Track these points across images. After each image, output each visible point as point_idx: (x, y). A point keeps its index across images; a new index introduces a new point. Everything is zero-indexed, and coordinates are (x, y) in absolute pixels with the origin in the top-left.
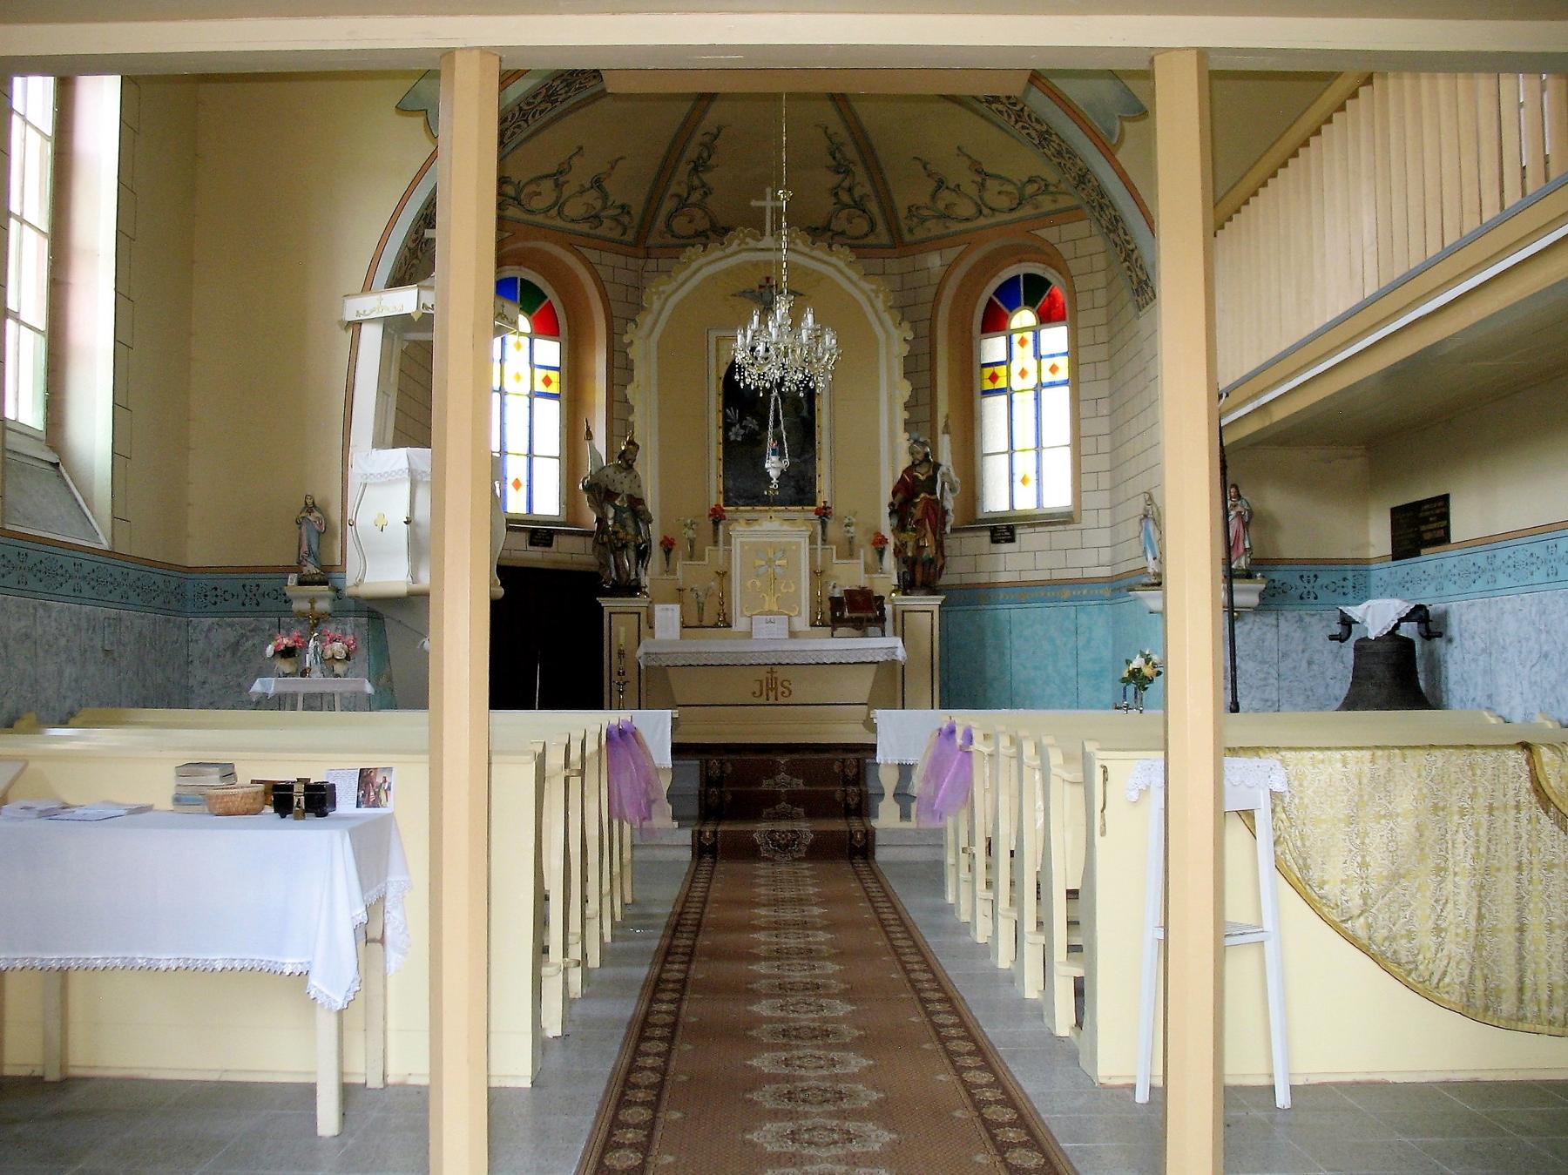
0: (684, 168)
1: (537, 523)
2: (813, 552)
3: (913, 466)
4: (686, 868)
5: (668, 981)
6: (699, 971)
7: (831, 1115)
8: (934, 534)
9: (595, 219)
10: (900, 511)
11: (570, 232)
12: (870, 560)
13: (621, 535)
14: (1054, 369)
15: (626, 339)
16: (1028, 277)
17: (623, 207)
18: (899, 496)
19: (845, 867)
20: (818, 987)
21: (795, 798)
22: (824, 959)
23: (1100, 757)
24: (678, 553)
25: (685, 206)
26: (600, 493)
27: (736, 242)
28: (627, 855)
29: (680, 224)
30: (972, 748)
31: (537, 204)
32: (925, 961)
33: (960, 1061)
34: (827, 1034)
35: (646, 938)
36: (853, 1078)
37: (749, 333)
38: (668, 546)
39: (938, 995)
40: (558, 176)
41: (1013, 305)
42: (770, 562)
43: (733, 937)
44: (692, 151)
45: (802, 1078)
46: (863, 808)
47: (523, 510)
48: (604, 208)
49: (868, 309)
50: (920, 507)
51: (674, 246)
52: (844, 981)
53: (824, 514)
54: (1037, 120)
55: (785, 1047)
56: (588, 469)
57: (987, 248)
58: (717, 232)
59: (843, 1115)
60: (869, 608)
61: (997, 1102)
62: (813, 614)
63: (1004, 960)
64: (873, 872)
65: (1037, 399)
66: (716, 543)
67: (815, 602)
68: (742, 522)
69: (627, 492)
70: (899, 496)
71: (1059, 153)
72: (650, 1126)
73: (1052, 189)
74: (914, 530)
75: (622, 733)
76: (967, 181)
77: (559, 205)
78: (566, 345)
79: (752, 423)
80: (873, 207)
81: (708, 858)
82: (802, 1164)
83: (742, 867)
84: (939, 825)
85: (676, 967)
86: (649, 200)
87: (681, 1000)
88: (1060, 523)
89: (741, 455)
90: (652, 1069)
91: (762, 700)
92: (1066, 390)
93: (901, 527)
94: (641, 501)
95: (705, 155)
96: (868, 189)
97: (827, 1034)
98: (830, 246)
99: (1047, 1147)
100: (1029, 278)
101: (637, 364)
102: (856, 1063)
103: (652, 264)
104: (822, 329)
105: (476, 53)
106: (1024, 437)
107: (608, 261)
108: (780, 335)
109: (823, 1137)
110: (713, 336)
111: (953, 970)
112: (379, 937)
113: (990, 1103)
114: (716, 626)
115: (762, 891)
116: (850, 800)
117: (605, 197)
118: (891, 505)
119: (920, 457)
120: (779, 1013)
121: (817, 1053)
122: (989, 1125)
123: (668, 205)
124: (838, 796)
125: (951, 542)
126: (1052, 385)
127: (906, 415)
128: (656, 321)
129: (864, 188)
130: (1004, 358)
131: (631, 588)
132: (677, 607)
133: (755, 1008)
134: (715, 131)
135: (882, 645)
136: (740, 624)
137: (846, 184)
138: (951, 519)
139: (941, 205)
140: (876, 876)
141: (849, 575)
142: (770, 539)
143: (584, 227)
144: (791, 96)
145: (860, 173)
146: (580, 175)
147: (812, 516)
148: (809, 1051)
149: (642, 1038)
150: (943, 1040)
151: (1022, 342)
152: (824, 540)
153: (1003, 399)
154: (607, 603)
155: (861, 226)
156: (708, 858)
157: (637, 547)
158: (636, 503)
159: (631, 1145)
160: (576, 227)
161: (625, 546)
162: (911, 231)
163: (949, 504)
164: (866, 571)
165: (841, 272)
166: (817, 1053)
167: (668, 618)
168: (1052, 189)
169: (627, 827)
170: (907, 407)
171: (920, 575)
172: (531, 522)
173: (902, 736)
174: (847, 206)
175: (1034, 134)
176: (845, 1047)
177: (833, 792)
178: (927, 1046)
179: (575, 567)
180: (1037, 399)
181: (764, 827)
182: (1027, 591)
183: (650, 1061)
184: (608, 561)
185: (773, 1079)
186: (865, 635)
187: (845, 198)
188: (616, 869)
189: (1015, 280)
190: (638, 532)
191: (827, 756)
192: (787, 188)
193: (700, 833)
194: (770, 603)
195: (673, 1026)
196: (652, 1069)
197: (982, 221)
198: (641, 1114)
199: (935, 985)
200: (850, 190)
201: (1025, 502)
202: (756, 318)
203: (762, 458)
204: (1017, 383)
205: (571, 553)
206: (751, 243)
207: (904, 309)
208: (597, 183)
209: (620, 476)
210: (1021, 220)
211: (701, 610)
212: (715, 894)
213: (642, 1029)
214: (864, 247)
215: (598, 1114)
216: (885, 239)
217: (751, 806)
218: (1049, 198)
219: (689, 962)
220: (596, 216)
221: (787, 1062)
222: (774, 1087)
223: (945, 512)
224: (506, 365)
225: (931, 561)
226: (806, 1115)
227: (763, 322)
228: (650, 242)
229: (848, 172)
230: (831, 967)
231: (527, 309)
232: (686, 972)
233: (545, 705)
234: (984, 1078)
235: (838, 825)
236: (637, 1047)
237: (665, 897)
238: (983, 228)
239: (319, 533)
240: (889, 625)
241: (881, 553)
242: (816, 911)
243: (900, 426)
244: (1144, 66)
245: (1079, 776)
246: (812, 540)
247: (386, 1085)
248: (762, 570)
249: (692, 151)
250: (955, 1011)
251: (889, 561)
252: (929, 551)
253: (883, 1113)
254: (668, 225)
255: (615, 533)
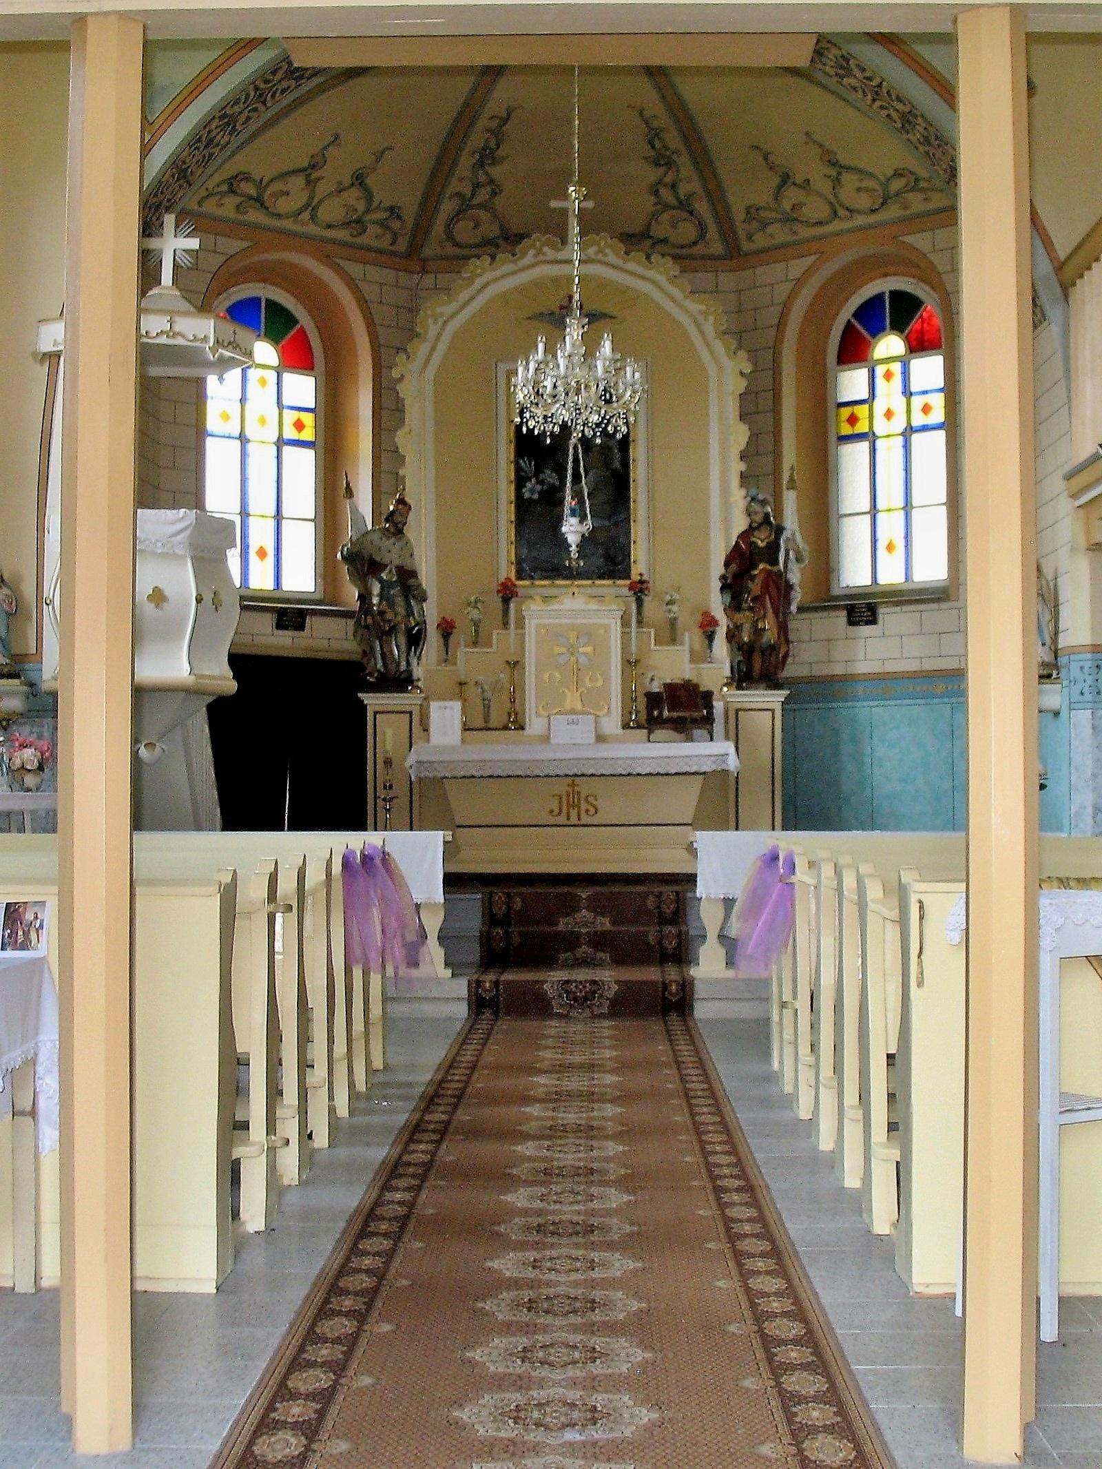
0: (466, 162)
1: (288, 601)
2: (625, 636)
3: (751, 530)
4: (458, 1026)
5: (409, 1164)
6: (449, 1153)
7: (575, 1329)
8: (776, 613)
9: (358, 224)
10: (734, 586)
11: (323, 240)
12: (697, 647)
13: (389, 616)
14: (926, 409)
15: (395, 374)
16: (894, 294)
17: (391, 209)
18: (734, 567)
19: (656, 1025)
20: (592, 1171)
21: (599, 941)
22: (607, 1138)
23: (918, 890)
24: (458, 637)
25: (470, 207)
26: (363, 564)
27: (532, 252)
28: (376, 1010)
29: (463, 231)
30: (794, 879)
31: (283, 205)
32: (730, 1141)
33: (749, 1264)
34: (591, 1229)
35: (391, 1111)
36: (612, 1283)
37: (532, 366)
38: (447, 630)
39: (737, 1183)
40: (310, 171)
41: (877, 330)
42: (572, 650)
43: (502, 1111)
44: (477, 139)
45: (548, 1284)
46: (680, 953)
47: (270, 585)
48: (368, 211)
49: (692, 331)
50: (758, 581)
51: (457, 258)
52: (625, 1166)
53: (640, 589)
54: (899, 99)
55: (536, 1246)
56: (349, 534)
57: (849, 256)
58: (509, 239)
59: (591, 1329)
60: (695, 707)
61: (785, 1314)
62: (626, 713)
63: (826, 1143)
64: (688, 1031)
65: (907, 447)
66: (506, 624)
67: (629, 698)
68: (538, 598)
69: (397, 562)
70: (734, 567)
71: (927, 141)
72: (352, 1341)
73: (922, 184)
74: (751, 609)
75: (367, 859)
76: (818, 174)
77: (311, 207)
78: (322, 379)
79: (550, 477)
80: (702, 207)
81: (488, 1014)
82: (529, 1388)
83: (531, 1025)
84: (763, 974)
85: (422, 1147)
86: (426, 197)
87: (419, 1188)
88: (932, 601)
89: (536, 515)
90: (368, 1272)
91: (562, 819)
92: (941, 435)
93: (735, 606)
94: (413, 574)
95: (492, 144)
96: (695, 186)
97: (591, 1229)
98: (648, 257)
99: (834, 1369)
100: (896, 296)
101: (408, 402)
102: (620, 1265)
103: (429, 280)
104: (623, 359)
105: (113, 18)
106: (891, 494)
107: (375, 277)
108: (570, 366)
109: (564, 1354)
110: (503, 368)
111: (763, 1153)
112: (28, 1108)
113: (775, 1315)
114: (506, 728)
115: (548, 1054)
116: (666, 943)
117: (369, 197)
118: (723, 577)
119: (759, 518)
120: (538, 1204)
121: (575, 1253)
122: (768, 1342)
123: (448, 207)
124: (652, 939)
125: (799, 626)
126: (925, 428)
127: (742, 466)
128: (433, 349)
129: (690, 184)
130: (865, 395)
131: (400, 682)
132: (457, 706)
133: (509, 1198)
134: (504, 115)
135: (710, 751)
136: (535, 725)
137: (668, 179)
138: (797, 597)
139: (787, 206)
140: (689, 1033)
141: (671, 665)
142: (573, 618)
143: (342, 235)
144: (587, 71)
145: (686, 166)
146: (337, 170)
147: (625, 591)
148: (564, 1251)
149: (364, 1233)
150: (733, 1238)
151: (888, 375)
152: (640, 622)
153: (864, 446)
154: (371, 701)
155: (687, 231)
156: (488, 1014)
157: (409, 630)
158: (407, 577)
159: (323, 1364)
160: (330, 234)
161: (393, 629)
162: (750, 238)
163: (795, 577)
164: (692, 661)
165: (660, 288)
166: (575, 1253)
167: (446, 719)
168: (922, 184)
169: (376, 980)
170: (743, 457)
171: (757, 666)
172: (279, 600)
173: (722, 864)
174: (667, 207)
175: (894, 115)
176: (610, 1246)
177: (646, 934)
178: (711, 1245)
179: (335, 656)
180: (907, 447)
181: (558, 975)
182: (888, 684)
183: (367, 1262)
184: (372, 649)
185: (516, 1284)
186: (690, 739)
187: (666, 195)
188: (358, 1026)
189: (879, 298)
190: (410, 613)
191: (640, 888)
192: (580, 183)
193: (478, 983)
194: (572, 700)
195: (404, 1221)
196: (368, 1272)
197: (837, 226)
198: (340, 1326)
199: (736, 1171)
200: (673, 186)
201: (891, 574)
202: (541, 347)
203: (559, 521)
204: (880, 426)
205: (329, 638)
206: (550, 253)
207: (741, 335)
208: (359, 179)
209: (387, 543)
210: (883, 224)
211: (487, 707)
212: (488, 1058)
213: (365, 1223)
214: (693, 258)
215: (291, 1326)
216: (717, 247)
217: (541, 952)
218: (920, 196)
219: (439, 1142)
220: (358, 221)
221: (535, 1265)
222: (513, 1294)
223: (790, 587)
224: (248, 406)
225: (773, 648)
226: (545, 1329)
227: (550, 350)
228: (427, 252)
229: (669, 164)
230: (613, 1148)
231: (273, 336)
232: (433, 1154)
233: (289, 830)
234: (773, 1284)
235: (651, 974)
236: (355, 1244)
237: (428, 1060)
238: (837, 234)
239: (9, 615)
240: (718, 726)
241: (710, 637)
242: (609, 1079)
243: (735, 481)
244: (946, 28)
245: (894, 914)
246: (625, 623)
247: (38, 1289)
248: (562, 660)
249: (477, 139)
250: (755, 1203)
251: (721, 647)
252: (770, 636)
253: (639, 1328)
254: (450, 236)
255: (382, 613)
